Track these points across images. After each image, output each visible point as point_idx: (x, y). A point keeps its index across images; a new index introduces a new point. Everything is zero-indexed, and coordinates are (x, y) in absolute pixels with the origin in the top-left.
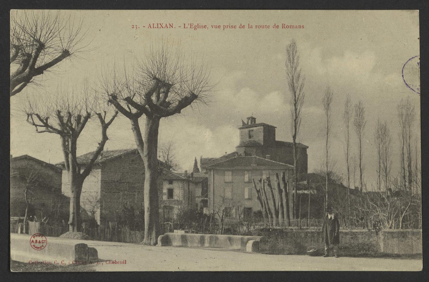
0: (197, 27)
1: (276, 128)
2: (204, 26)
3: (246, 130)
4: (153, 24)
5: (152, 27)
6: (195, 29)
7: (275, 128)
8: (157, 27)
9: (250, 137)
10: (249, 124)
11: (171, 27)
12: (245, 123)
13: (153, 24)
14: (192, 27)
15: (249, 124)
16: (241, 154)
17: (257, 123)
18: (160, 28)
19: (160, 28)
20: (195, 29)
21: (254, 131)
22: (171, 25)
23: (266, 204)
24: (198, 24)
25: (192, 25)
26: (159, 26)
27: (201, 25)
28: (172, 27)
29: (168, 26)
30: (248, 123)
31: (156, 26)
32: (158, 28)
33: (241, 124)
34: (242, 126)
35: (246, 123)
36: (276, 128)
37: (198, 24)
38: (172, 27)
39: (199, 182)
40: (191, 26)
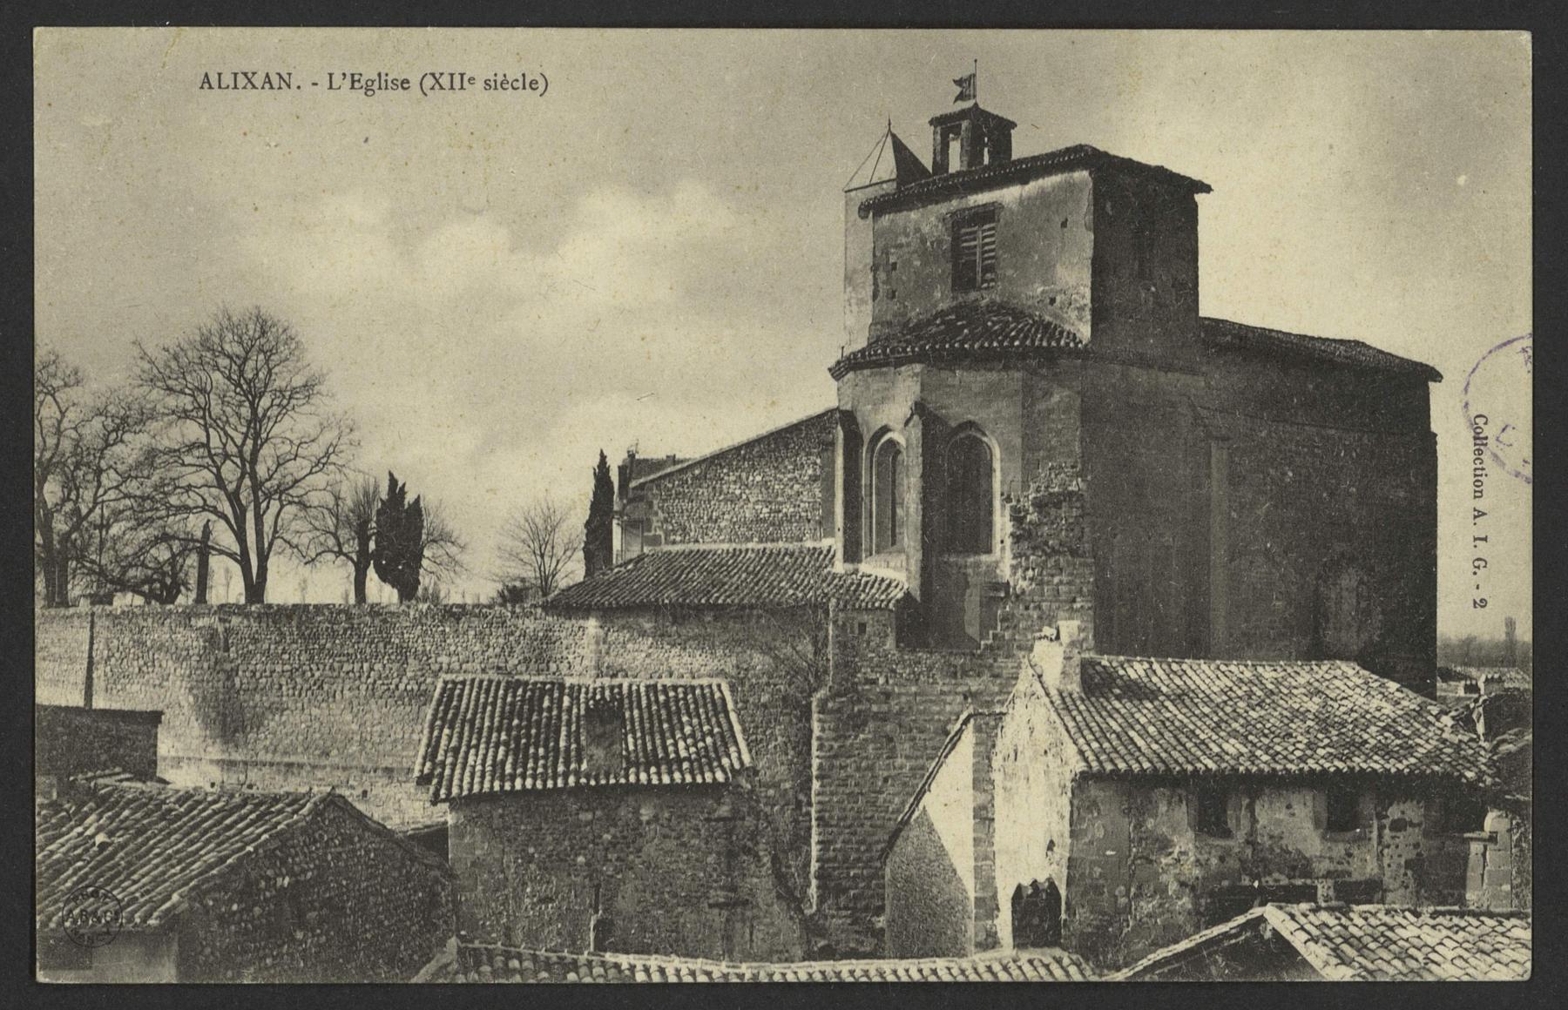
0: (376, 84)
1: (1207, 189)
2: (402, 83)
3: (927, 220)
4: (220, 74)
5: (214, 83)
6: (370, 93)
7: (1199, 198)
8: (232, 85)
9: (965, 274)
10: (955, 164)
11: (283, 85)
12: (916, 161)
13: (220, 74)
14: (357, 85)
15: (955, 164)
16: (885, 429)
17: (1023, 146)
18: (245, 88)
19: (245, 88)
20: (368, 90)
21: (1003, 217)
22: (286, 77)
23: (478, 774)
24: (379, 75)
25: (356, 77)
26: (242, 81)
27: (390, 79)
28: (289, 86)
29: (275, 80)
30: (941, 164)
31: (227, 80)
32: (236, 87)
33: (887, 167)
34: (890, 188)
35: (927, 161)
36: (1207, 189)
37: (379, 75)
38: (289, 86)
39: (1390, 788)
40: (353, 82)
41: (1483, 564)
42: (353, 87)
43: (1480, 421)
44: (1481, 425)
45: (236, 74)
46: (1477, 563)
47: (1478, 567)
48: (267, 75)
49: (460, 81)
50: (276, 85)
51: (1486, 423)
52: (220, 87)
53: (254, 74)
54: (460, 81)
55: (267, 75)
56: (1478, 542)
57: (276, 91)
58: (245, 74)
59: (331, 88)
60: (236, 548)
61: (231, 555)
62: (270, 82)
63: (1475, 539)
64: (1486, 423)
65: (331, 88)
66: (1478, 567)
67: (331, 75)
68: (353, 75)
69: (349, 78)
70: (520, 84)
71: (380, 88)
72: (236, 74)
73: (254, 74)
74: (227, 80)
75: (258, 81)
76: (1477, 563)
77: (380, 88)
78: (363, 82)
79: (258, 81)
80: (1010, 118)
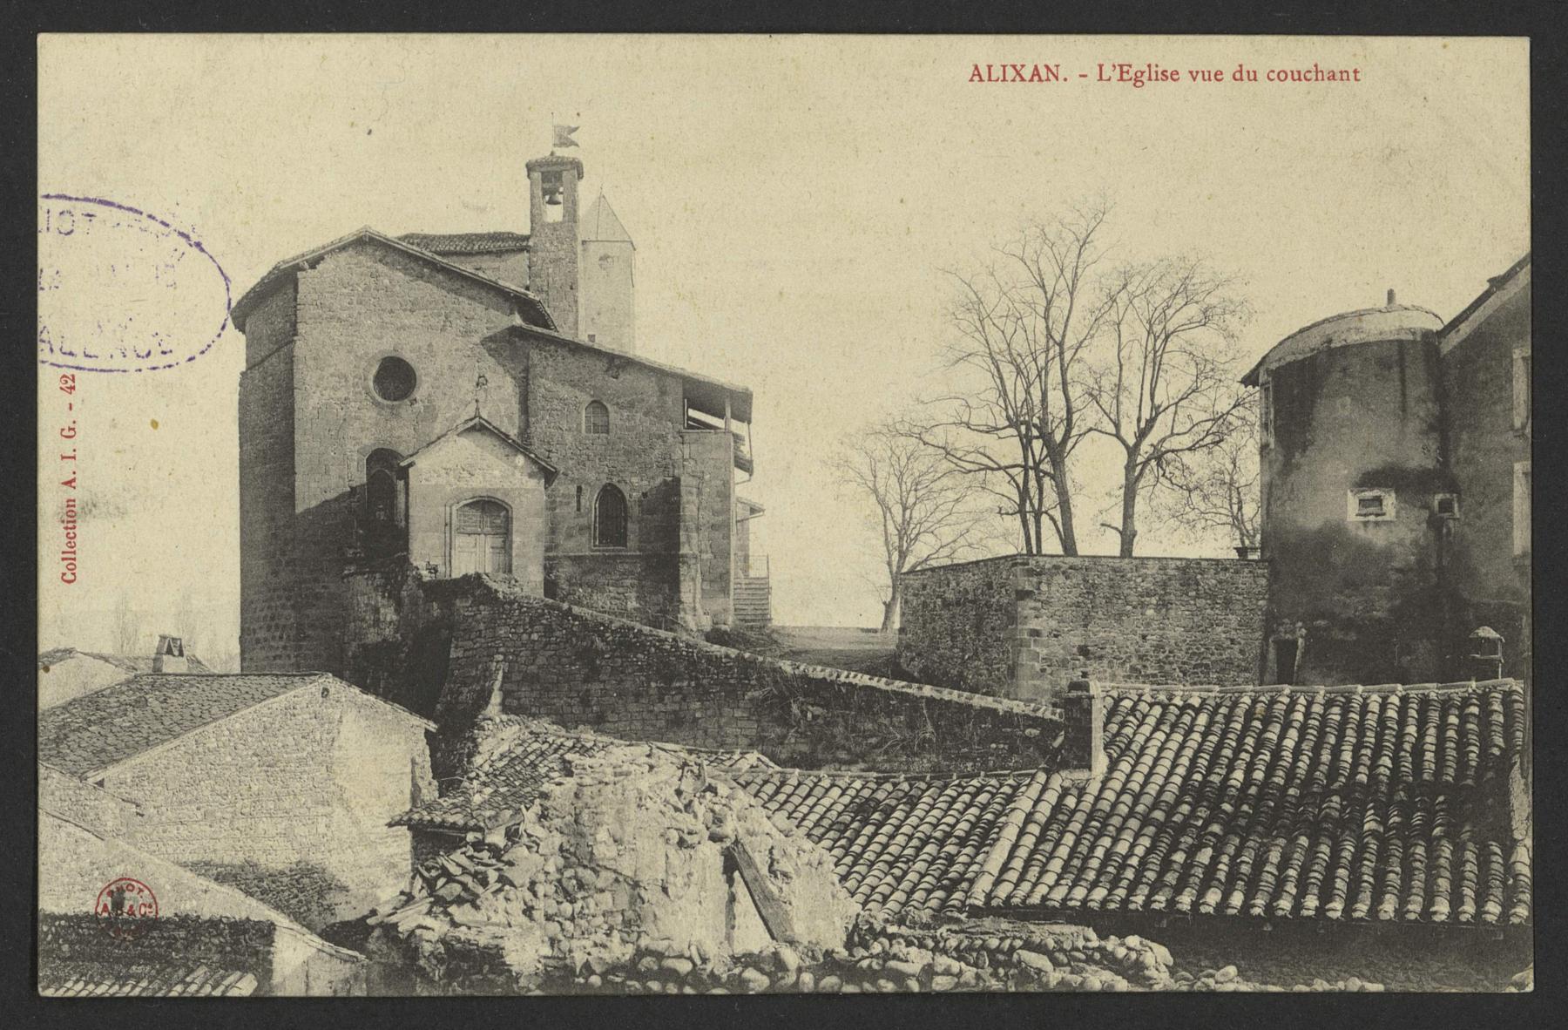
0: (1146, 75)
5: (985, 76)
6: (1139, 84)
11: (1051, 76)
18: (1013, 80)
19: (1013, 80)
25: (1125, 69)
27: (1160, 70)
28: (1057, 78)
29: (1043, 72)
31: (997, 72)
32: (1004, 80)
37: (1149, 66)
38: (1057, 78)
40: (1122, 72)
41: (65, 433)
42: (1122, 79)
43: (69, 577)
44: (69, 573)
45: (1004, 67)
46: (72, 433)
47: (70, 429)
48: (1036, 68)
49: (1171, 76)
50: (1044, 77)
51: (64, 574)
52: (990, 80)
53: (1023, 66)
54: (1171, 76)
55: (1036, 68)
56: (72, 454)
57: (1027, 83)
58: (1014, 67)
59: (1101, 79)
60: (1131, 441)
61: (1127, 446)
62: (1038, 75)
63: (74, 458)
64: (64, 574)
65: (1101, 79)
66: (70, 429)
67: (1101, 66)
68: (1121, 66)
69: (1118, 69)
70: (1313, 75)
71: (1150, 79)
72: (1004, 67)
73: (1023, 66)
74: (997, 72)
75: (1027, 73)
76: (72, 433)
77: (1150, 79)
78: (1132, 74)
79: (1027, 73)
80: (755, 415)
